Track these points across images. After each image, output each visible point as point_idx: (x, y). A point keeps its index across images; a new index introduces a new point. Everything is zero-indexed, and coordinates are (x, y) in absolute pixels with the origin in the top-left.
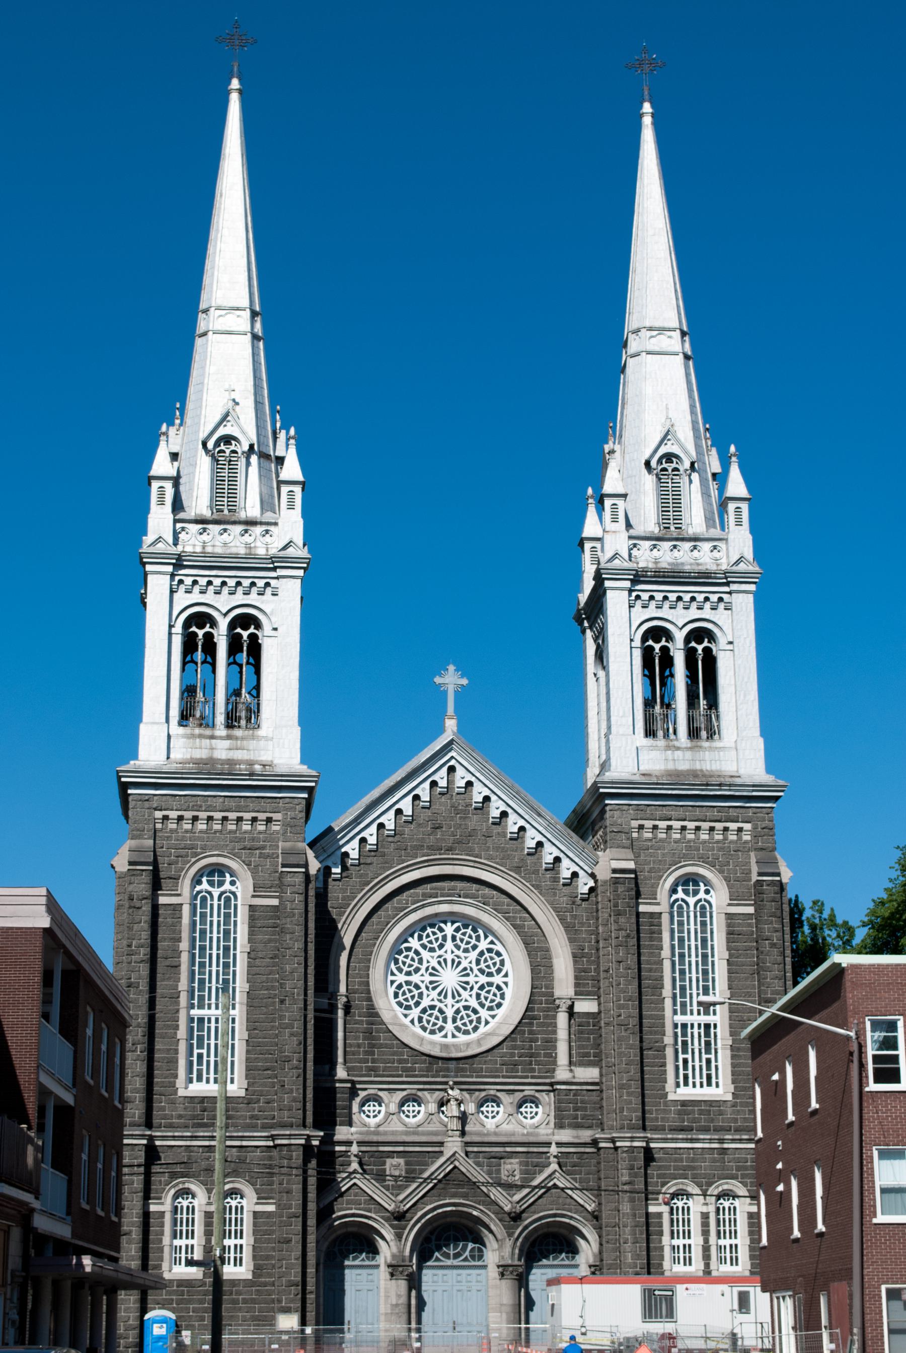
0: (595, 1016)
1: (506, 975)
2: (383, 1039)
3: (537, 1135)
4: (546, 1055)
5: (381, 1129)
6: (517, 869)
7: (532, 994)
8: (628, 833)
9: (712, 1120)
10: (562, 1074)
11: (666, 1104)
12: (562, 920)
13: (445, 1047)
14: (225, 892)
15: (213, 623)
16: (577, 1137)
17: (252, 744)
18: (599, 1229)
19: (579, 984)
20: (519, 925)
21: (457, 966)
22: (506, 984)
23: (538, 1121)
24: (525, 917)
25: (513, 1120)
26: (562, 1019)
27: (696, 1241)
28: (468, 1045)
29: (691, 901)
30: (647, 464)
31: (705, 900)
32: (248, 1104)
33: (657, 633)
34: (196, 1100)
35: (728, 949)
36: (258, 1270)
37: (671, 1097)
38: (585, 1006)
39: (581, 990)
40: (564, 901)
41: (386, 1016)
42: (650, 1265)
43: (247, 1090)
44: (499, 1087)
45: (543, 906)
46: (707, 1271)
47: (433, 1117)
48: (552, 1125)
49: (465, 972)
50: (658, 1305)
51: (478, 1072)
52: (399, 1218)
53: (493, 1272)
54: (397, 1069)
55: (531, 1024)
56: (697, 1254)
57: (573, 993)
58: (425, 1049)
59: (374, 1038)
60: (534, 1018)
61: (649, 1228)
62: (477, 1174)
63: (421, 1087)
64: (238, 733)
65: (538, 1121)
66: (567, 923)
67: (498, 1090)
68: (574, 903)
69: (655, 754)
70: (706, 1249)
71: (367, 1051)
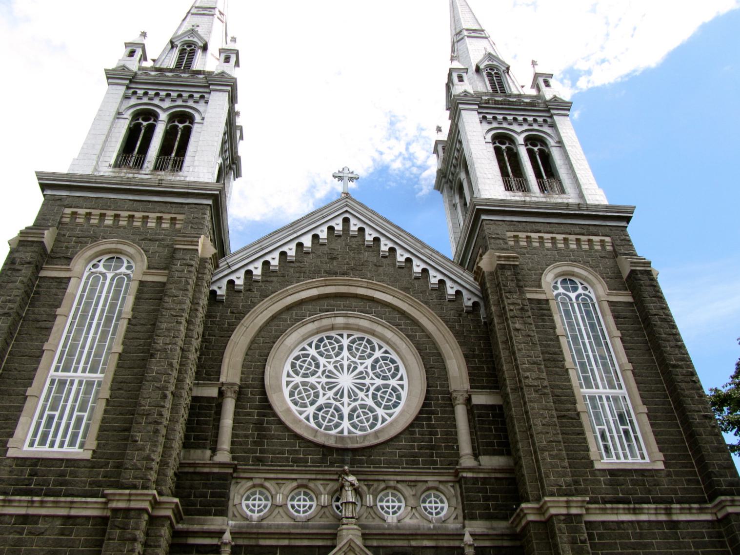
1: (401, 379)
2: (274, 430)
3: (446, 529)
4: (446, 447)
5: (264, 522)
6: (406, 289)
7: (428, 392)
9: (649, 492)
10: (467, 461)
11: (594, 472)
12: (451, 328)
14: (120, 274)
16: (493, 528)
19: (474, 380)
20: (411, 335)
21: (353, 371)
22: (402, 386)
23: (440, 510)
24: (415, 329)
25: (417, 514)
26: (461, 413)
29: (573, 295)
31: (585, 295)
32: (93, 467)
34: (28, 463)
35: (618, 329)
37: (597, 466)
38: (480, 399)
39: (476, 382)
43: (94, 451)
44: (399, 478)
45: (435, 321)
47: (326, 510)
48: (461, 518)
51: (376, 463)
54: (287, 459)
55: (429, 419)
57: (469, 387)
59: (265, 429)
60: (432, 412)
63: (313, 476)
65: (440, 510)
66: (456, 330)
67: (398, 482)
68: (460, 315)
71: (255, 442)
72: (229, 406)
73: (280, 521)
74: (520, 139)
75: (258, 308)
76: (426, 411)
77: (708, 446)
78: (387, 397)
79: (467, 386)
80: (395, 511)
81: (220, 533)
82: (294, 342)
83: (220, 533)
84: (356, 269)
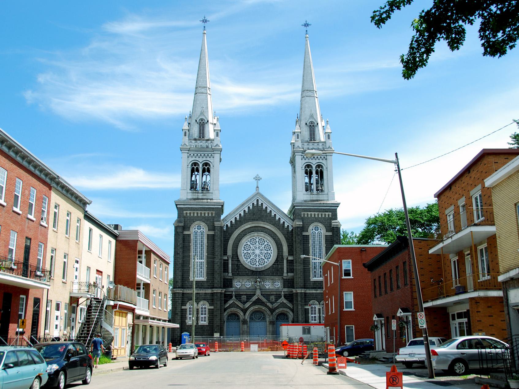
0: (293, 260)
8: (300, 215)
10: (285, 274)
13: (256, 268)
15: (198, 165)
17: (208, 194)
18: (293, 312)
26: (285, 261)
27: (317, 315)
28: (262, 268)
30: (306, 124)
33: (308, 166)
36: (209, 323)
38: (290, 258)
40: (286, 232)
41: (242, 261)
42: (306, 321)
46: (320, 322)
49: (261, 250)
50: (307, 331)
52: (272, 311)
53: (268, 323)
56: (317, 318)
58: (251, 269)
61: (306, 311)
62: (264, 300)
64: (205, 192)
69: (308, 196)
70: (320, 317)
72: (230, 261)
73: (244, 288)
74: (314, 167)
75: (235, 232)
76: (277, 261)
77: (319, 332)
78: (267, 256)
79: (287, 254)
80: (268, 285)
81: (232, 292)
82: (245, 241)
83: (232, 292)
84: (260, 219)
